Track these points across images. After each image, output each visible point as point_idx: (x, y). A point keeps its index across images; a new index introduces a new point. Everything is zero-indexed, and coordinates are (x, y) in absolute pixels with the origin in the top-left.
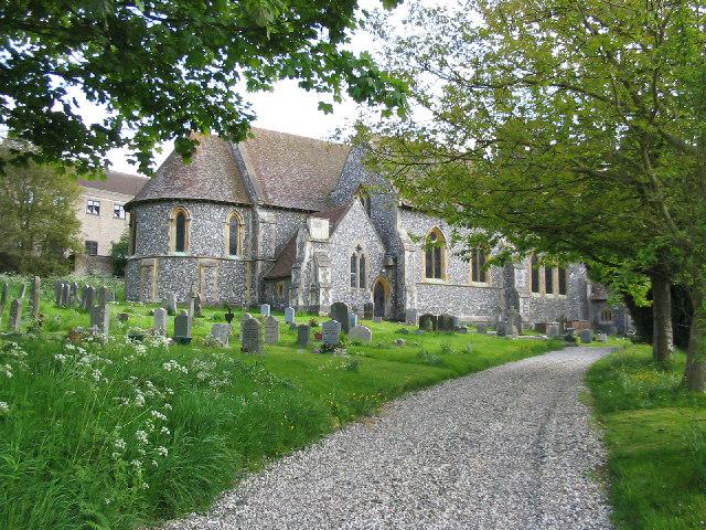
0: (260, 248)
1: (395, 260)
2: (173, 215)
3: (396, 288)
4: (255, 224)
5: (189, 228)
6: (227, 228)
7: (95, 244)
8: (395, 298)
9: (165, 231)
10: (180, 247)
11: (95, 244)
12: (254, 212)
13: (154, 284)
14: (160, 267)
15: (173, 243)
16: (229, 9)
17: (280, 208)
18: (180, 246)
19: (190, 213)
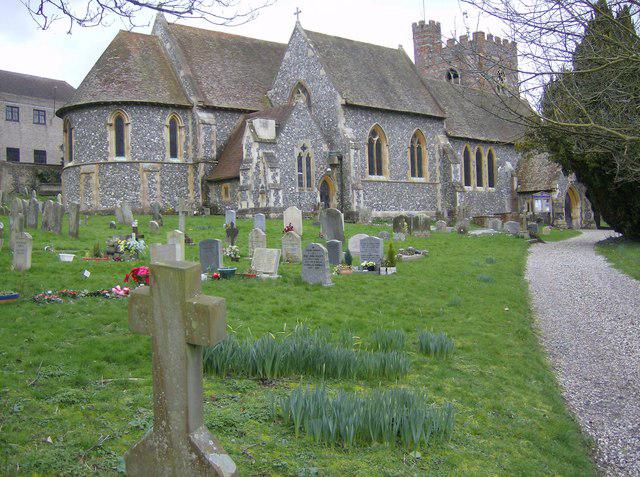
0: (202, 150)
2: (111, 120)
3: (342, 186)
5: (128, 131)
9: (104, 136)
10: (120, 152)
14: (101, 174)
15: (112, 149)
19: (128, 118)
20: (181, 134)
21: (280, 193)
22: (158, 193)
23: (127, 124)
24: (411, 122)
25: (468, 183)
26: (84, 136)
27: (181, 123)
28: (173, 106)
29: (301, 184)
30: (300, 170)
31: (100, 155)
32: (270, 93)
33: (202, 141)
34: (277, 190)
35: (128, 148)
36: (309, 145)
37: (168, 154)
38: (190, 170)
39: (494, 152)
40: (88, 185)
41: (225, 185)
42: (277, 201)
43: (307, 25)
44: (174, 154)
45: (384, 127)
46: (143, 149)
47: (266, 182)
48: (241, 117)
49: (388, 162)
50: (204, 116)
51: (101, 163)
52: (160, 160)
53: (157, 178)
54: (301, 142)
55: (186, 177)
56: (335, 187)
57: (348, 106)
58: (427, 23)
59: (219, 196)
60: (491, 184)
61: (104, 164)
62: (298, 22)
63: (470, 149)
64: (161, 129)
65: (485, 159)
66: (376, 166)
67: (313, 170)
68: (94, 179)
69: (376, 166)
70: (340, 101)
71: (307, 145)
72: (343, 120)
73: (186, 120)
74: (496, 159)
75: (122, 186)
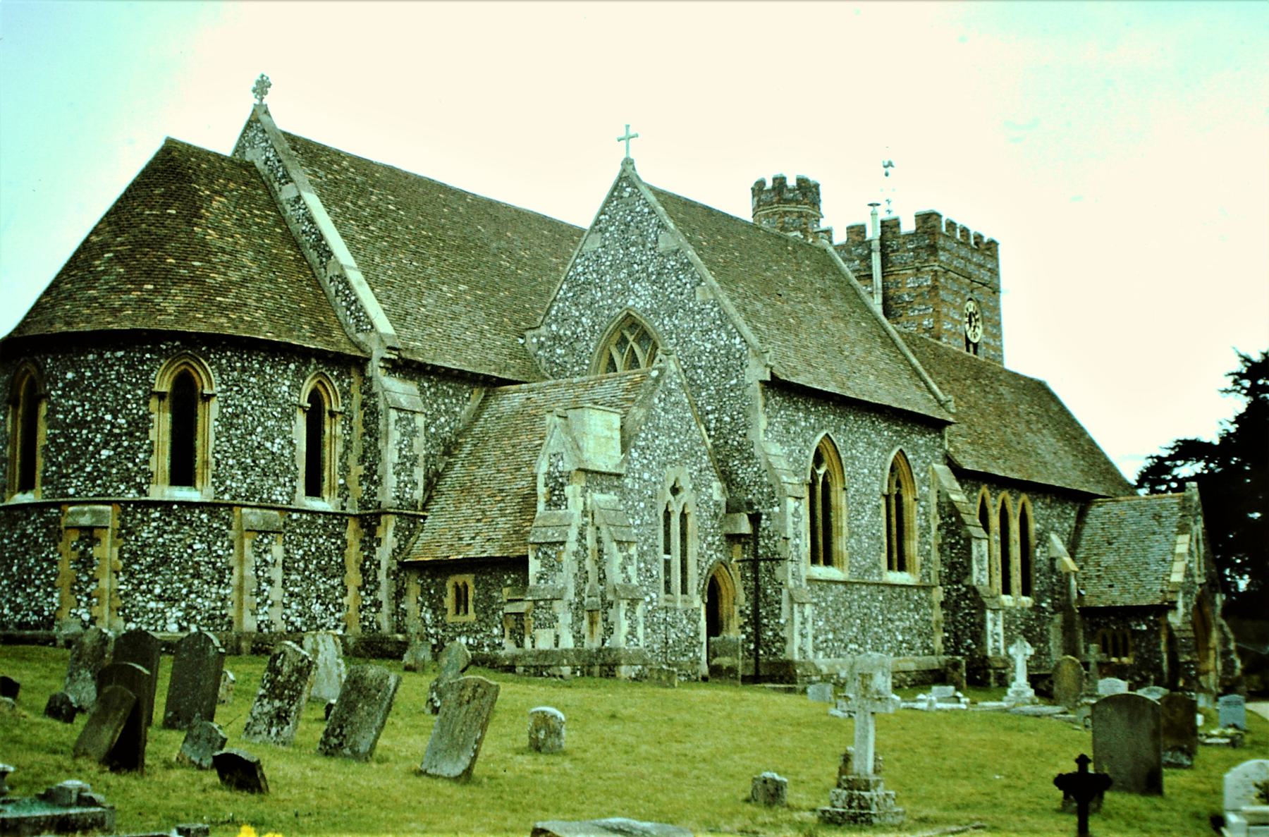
0: (391, 481)
1: (755, 519)
2: (163, 384)
3: (756, 594)
4: (371, 413)
5: (210, 418)
6: (301, 421)
7: (808, 191)
8: (755, 621)
9: (141, 425)
10: (182, 473)
11: (808, 191)
12: (367, 380)
13: (105, 583)
14: (125, 532)
15: (161, 462)
16: (2, 418)
17: (435, 370)
18: (182, 473)
19: (210, 381)
20: (333, 430)
21: (640, 610)
22: (276, 593)
23: (207, 398)
24: (887, 431)
25: (1007, 590)
26: (81, 424)
27: (334, 403)
28: (321, 356)
29: (668, 590)
30: (667, 551)
31: (127, 478)
32: (532, 340)
33: (391, 456)
34: (633, 602)
35: (206, 463)
36: (686, 484)
37: (301, 484)
38: (352, 533)
39: (1029, 507)
40: (85, 562)
41: (460, 579)
42: (632, 632)
43: (652, 174)
44: (314, 488)
45: (840, 440)
46: (245, 470)
47: (602, 580)
48: (477, 396)
49: (845, 531)
50: (399, 390)
51: (128, 503)
52: (283, 500)
53: (277, 551)
54: (670, 474)
55: (341, 550)
56: (737, 600)
57: (777, 386)
58: (791, 182)
59: (437, 607)
60: (1026, 591)
61: (138, 504)
62: (628, 162)
63: (990, 501)
64: (288, 417)
65: (1015, 526)
66: (823, 552)
67: (693, 549)
68: (106, 551)
69: (823, 552)
70: (756, 373)
71: (681, 484)
72: (763, 423)
73: (346, 394)
74: (1034, 527)
75: (183, 570)
